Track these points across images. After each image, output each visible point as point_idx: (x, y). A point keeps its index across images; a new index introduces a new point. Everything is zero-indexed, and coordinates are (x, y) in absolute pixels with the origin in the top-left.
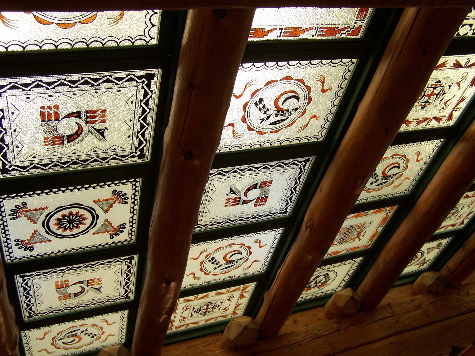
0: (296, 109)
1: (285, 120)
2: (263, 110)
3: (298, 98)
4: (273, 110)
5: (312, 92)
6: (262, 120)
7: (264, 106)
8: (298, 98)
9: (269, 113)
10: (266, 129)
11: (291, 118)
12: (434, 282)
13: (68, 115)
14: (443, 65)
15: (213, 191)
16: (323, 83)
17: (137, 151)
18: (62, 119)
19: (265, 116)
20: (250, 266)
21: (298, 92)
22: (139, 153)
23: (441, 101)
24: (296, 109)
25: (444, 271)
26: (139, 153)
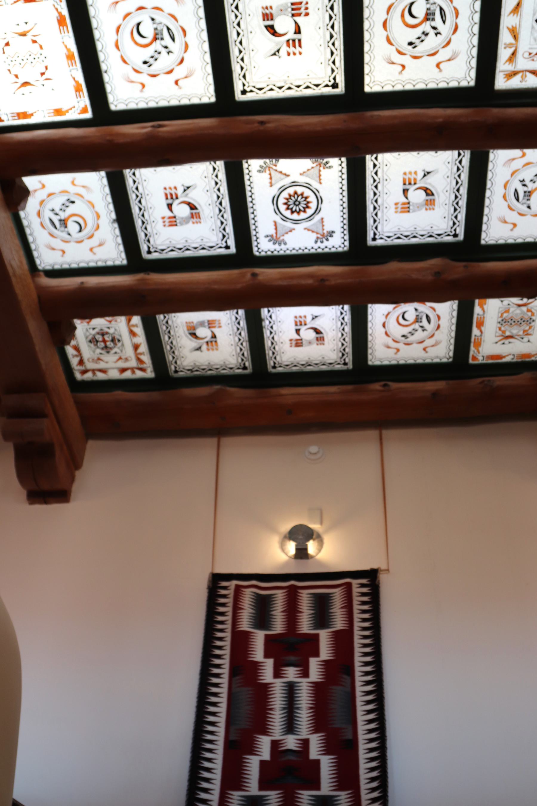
1: (56, 228)
4: (63, 215)
8: (80, 231)
20: (53, 249)
22: (454, 232)
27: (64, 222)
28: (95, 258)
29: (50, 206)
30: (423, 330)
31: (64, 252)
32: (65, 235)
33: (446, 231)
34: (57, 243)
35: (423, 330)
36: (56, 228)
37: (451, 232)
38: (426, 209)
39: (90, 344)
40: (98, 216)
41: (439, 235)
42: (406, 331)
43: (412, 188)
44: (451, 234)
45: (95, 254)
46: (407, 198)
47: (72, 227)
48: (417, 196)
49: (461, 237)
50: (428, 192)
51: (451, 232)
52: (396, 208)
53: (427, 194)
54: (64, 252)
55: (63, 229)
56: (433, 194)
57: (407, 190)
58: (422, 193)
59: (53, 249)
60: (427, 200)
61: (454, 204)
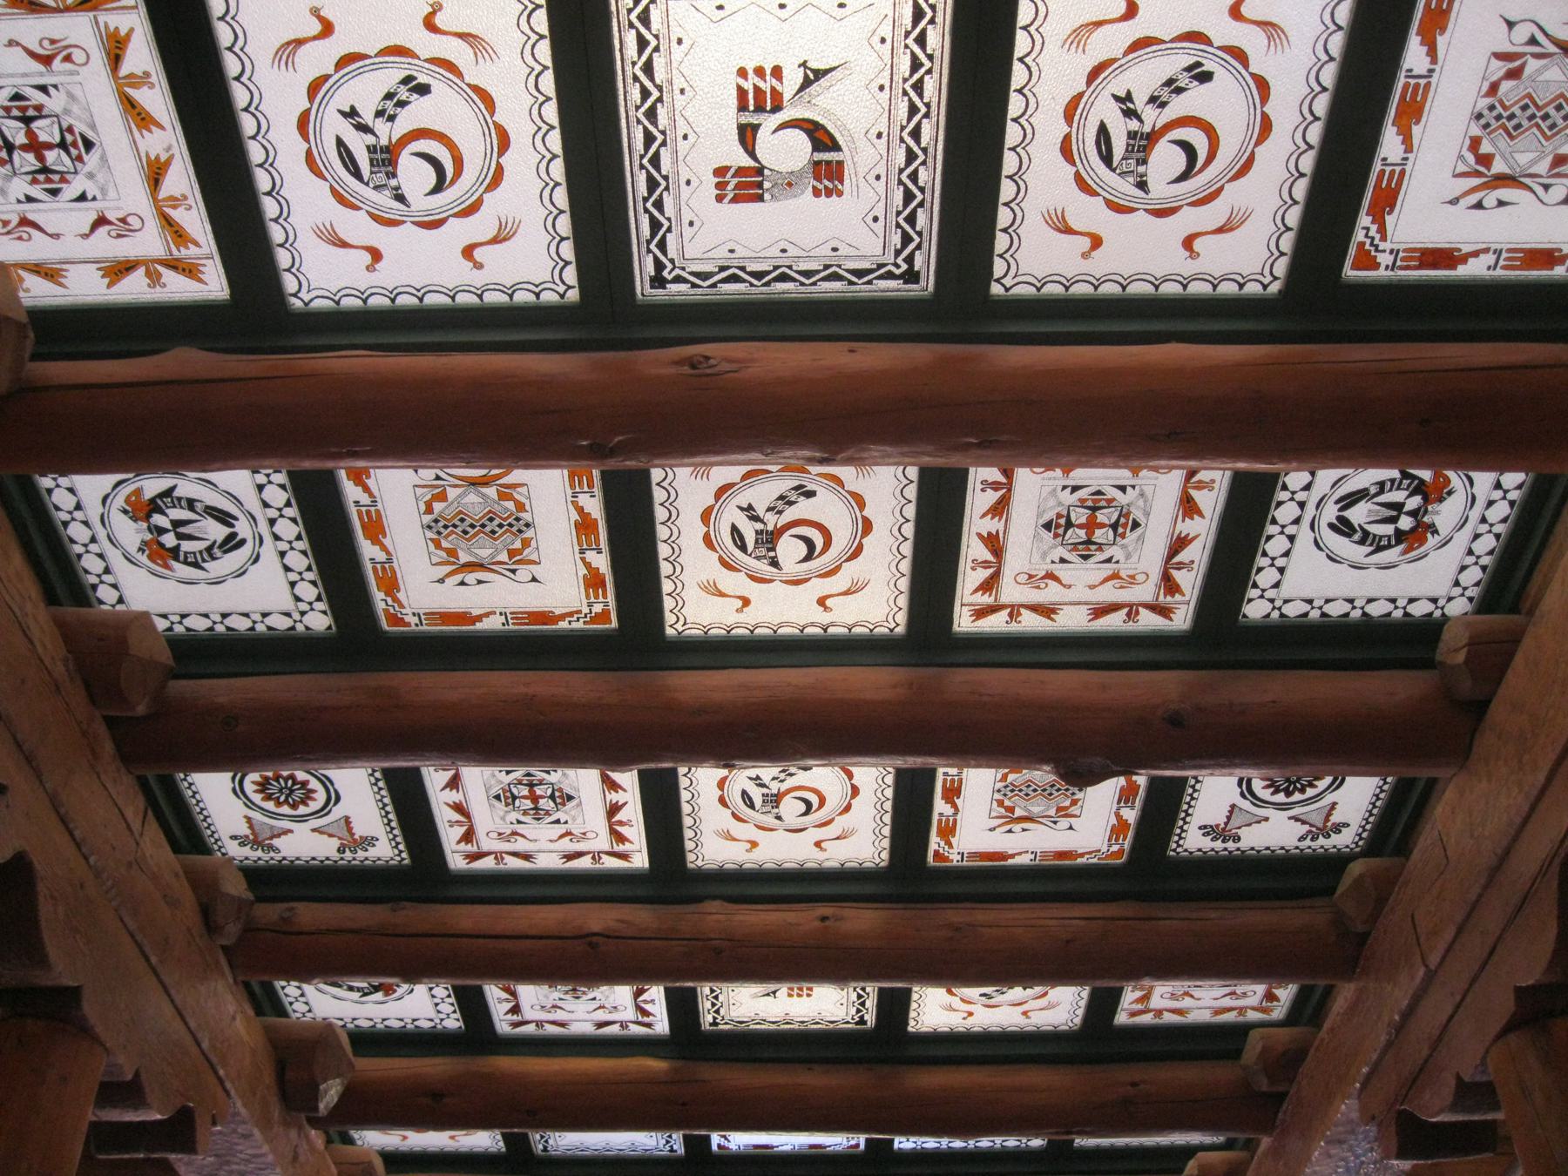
0: (400, 198)
1: (357, 174)
2: (389, 104)
3: (438, 188)
4: (385, 132)
5: (1072, 176)
6: (352, 113)
7: (402, 104)
8: (438, 188)
9: (381, 127)
10: (319, 133)
11: (368, 192)
12: (233, 897)
13: (746, 150)
14: (613, 786)
15: (870, 216)
16: (495, 240)
17: (899, 261)
18: (755, 159)
19: (367, 117)
20: (344, 245)
21: (458, 184)
22: (904, 267)
23: (519, 822)
24: (400, 198)
25: (269, 913)
26: (904, 267)
27: (386, 158)
28: (478, 279)
29: (342, 100)
30: (750, 507)
31: (376, 255)
32: (384, 200)
33: (881, 260)
34: (357, 227)
35: (750, 507)
36: (357, 174)
37: (898, 266)
38: (817, 193)
39: (1141, 519)
40: (505, 141)
41: (859, 273)
42: (803, 508)
43: (769, 122)
44: (898, 272)
45: (478, 266)
46: (752, 154)
47: (414, 174)
48: (785, 151)
49: (928, 284)
50: (821, 138)
51: (898, 266)
52: (720, 186)
53: (818, 146)
54: (376, 255)
55: (380, 178)
56: (836, 147)
57: (755, 128)
58: (800, 139)
59: (344, 245)
60: (817, 164)
61: (904, 177)
